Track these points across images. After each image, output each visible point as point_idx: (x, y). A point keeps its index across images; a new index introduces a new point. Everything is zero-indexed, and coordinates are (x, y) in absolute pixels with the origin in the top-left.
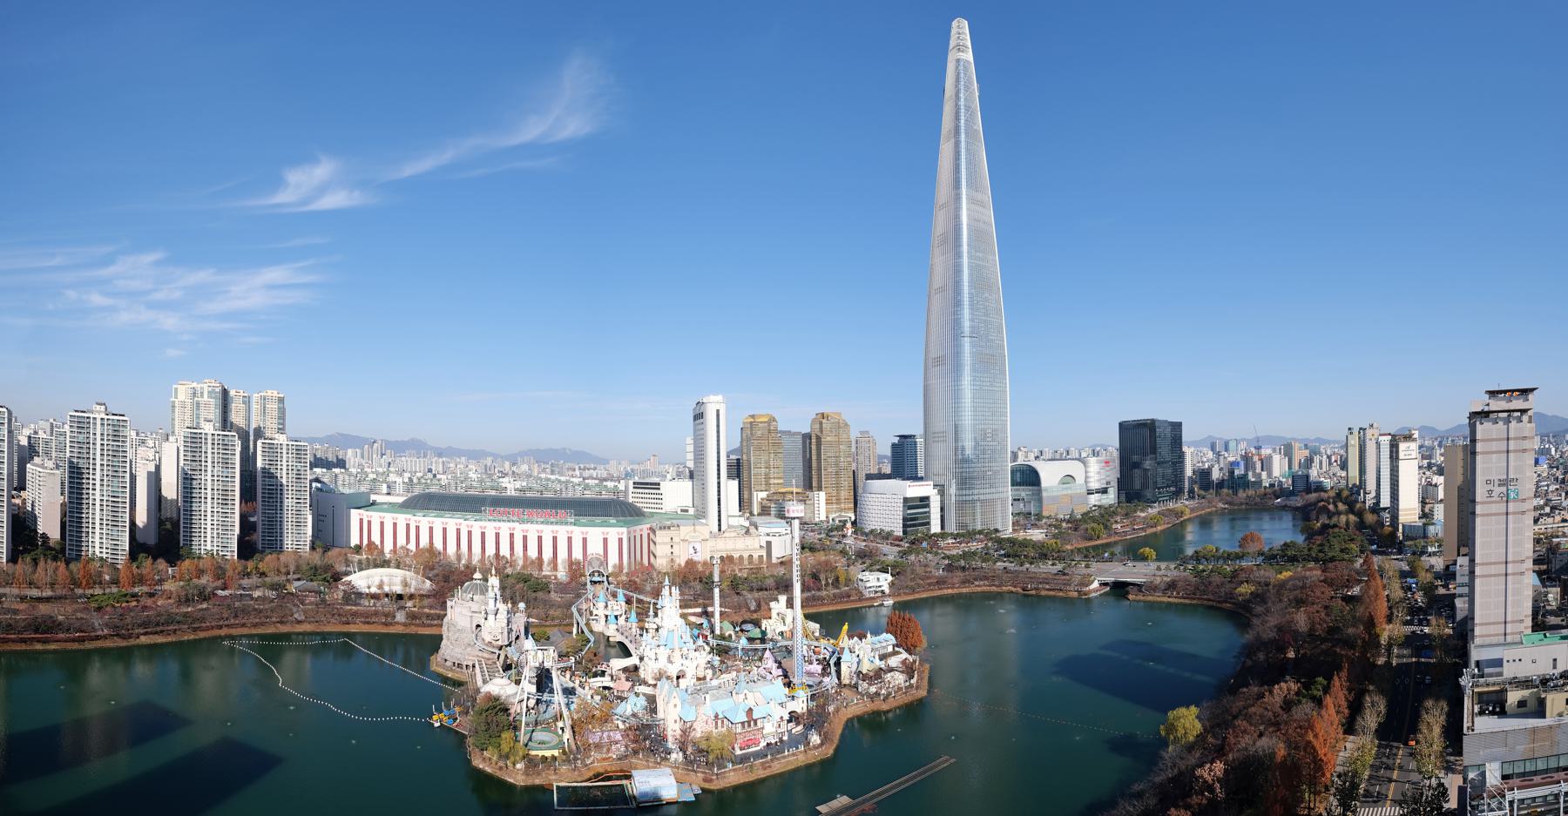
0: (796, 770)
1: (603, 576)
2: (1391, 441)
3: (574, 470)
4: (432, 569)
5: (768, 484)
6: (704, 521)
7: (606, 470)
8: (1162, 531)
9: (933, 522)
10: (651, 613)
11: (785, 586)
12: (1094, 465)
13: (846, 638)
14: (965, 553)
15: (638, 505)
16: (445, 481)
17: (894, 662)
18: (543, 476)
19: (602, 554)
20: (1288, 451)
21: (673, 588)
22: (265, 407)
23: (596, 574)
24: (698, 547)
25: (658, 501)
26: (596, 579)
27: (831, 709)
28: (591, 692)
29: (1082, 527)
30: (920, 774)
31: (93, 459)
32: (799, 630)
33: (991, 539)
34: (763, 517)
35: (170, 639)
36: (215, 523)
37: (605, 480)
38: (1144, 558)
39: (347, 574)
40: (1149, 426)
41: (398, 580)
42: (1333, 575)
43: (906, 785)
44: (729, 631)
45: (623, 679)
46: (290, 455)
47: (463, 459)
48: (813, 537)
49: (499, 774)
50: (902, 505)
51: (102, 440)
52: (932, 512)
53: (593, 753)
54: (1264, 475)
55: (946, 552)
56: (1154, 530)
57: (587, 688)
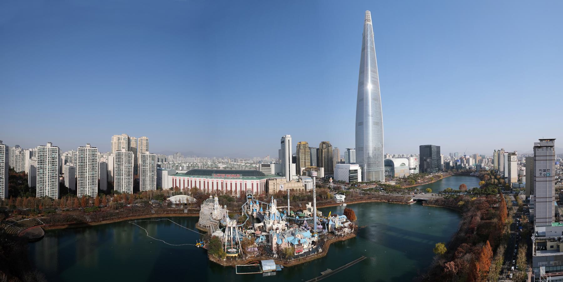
0: (314, 260)
1: (252, 196)
2: (508, 155)
3: (242, 161)
5: (305, 165)
6: (284, 177)
8: (434, 182)
9: (358, 178)
10: (267, 208)
12: (412, 160)
13: (330, 216)
14: (369, 189)
15: (263, 172)
18: (232, 163)
19: (251, 188)
20: (475, 157)
21: (275, 200)
22: (142, 143)
23: (250, 195)
24: (283, 186)
25: (270, 171)
26: (250, 197)
27: (325, 240)
28: (248, 235)
29: (408, 181)
33: (378, 184)
34: (304, 176)
35: (111, 222)
36: (126, 182)
37: (253, 164)
38: (428, 192)
39: (169, 197)
40: (430, 147)
41: (185, 199)
44: (293, 214)
45: (258, 230)
46: (150, 159)
48: (320, 183)
49: (218, 262)
51: (89, 156)
52: (358, 175)
54: (467, 165)
56: (431, 182)
57: (247, 233)
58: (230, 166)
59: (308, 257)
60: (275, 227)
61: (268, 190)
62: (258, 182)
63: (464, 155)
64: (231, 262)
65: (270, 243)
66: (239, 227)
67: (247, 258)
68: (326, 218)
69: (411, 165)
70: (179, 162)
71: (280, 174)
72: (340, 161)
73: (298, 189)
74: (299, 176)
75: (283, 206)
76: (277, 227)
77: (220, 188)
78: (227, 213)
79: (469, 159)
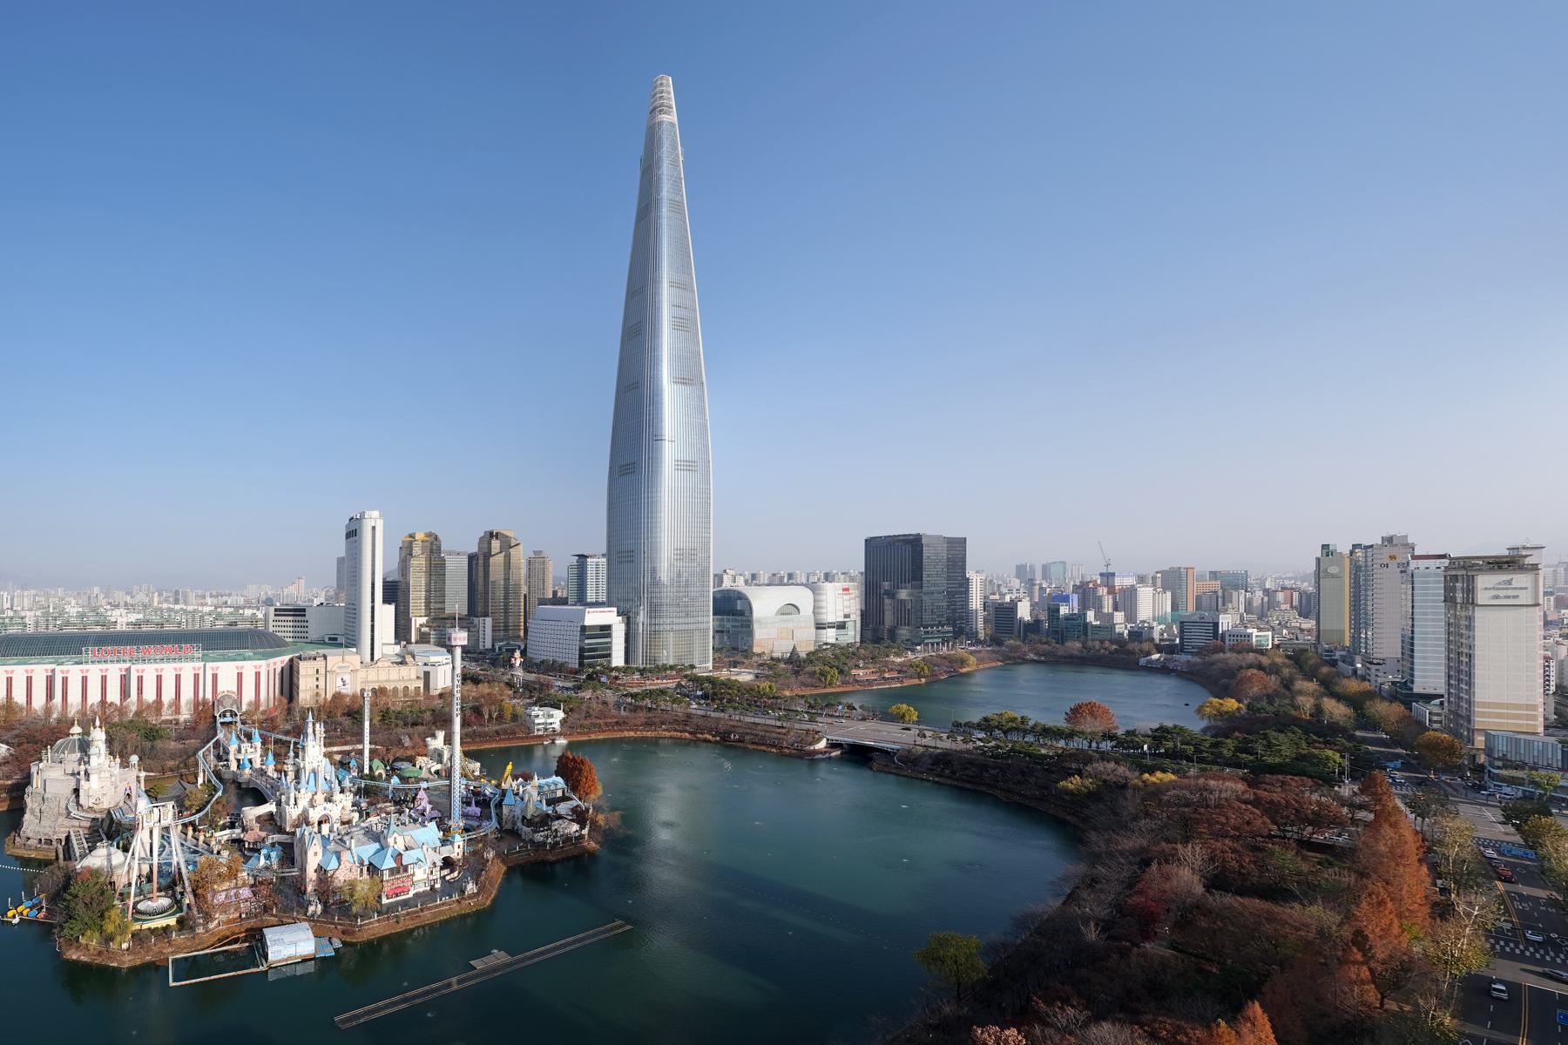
1: (236, 715)
3: (204, 597)
6: (354, 650)
7: (242, 596)
9: (614, 655)
10: (292, 754)
11: (443, 721)
13: (510, 779)
15: (280, 634)
17: (563, 808)
18: (165, 606)
19: (235, 690)
21: (318, 725)
23: (228, 714)
24: (347, 678)
26: (228, 719)
32: (457, 768)
33: (686, 676)
37: (243, 608)
40: (914, 544)
42: (1276, 797)
44: (380, 770)
49: (98, 960)
50: (579, 633)
53: (217, 915)
54: (1119, 617)
58: (155, 618)
59: (429, 909)
60: (315, 815)
61: (295, 694)
62: (260, 667)
63: (1101, 575)
64: (149, 950)
65: (296, 869)
66: (185, 826)
67: (212, 926)
68: (493, 782)
69: (824, 611)
72: (551, 596)
74: (405, 647)
75: (346, 744)
76: (325, 815)
77: (114, 696)
78: (139, 782)
79: (1130, 593)
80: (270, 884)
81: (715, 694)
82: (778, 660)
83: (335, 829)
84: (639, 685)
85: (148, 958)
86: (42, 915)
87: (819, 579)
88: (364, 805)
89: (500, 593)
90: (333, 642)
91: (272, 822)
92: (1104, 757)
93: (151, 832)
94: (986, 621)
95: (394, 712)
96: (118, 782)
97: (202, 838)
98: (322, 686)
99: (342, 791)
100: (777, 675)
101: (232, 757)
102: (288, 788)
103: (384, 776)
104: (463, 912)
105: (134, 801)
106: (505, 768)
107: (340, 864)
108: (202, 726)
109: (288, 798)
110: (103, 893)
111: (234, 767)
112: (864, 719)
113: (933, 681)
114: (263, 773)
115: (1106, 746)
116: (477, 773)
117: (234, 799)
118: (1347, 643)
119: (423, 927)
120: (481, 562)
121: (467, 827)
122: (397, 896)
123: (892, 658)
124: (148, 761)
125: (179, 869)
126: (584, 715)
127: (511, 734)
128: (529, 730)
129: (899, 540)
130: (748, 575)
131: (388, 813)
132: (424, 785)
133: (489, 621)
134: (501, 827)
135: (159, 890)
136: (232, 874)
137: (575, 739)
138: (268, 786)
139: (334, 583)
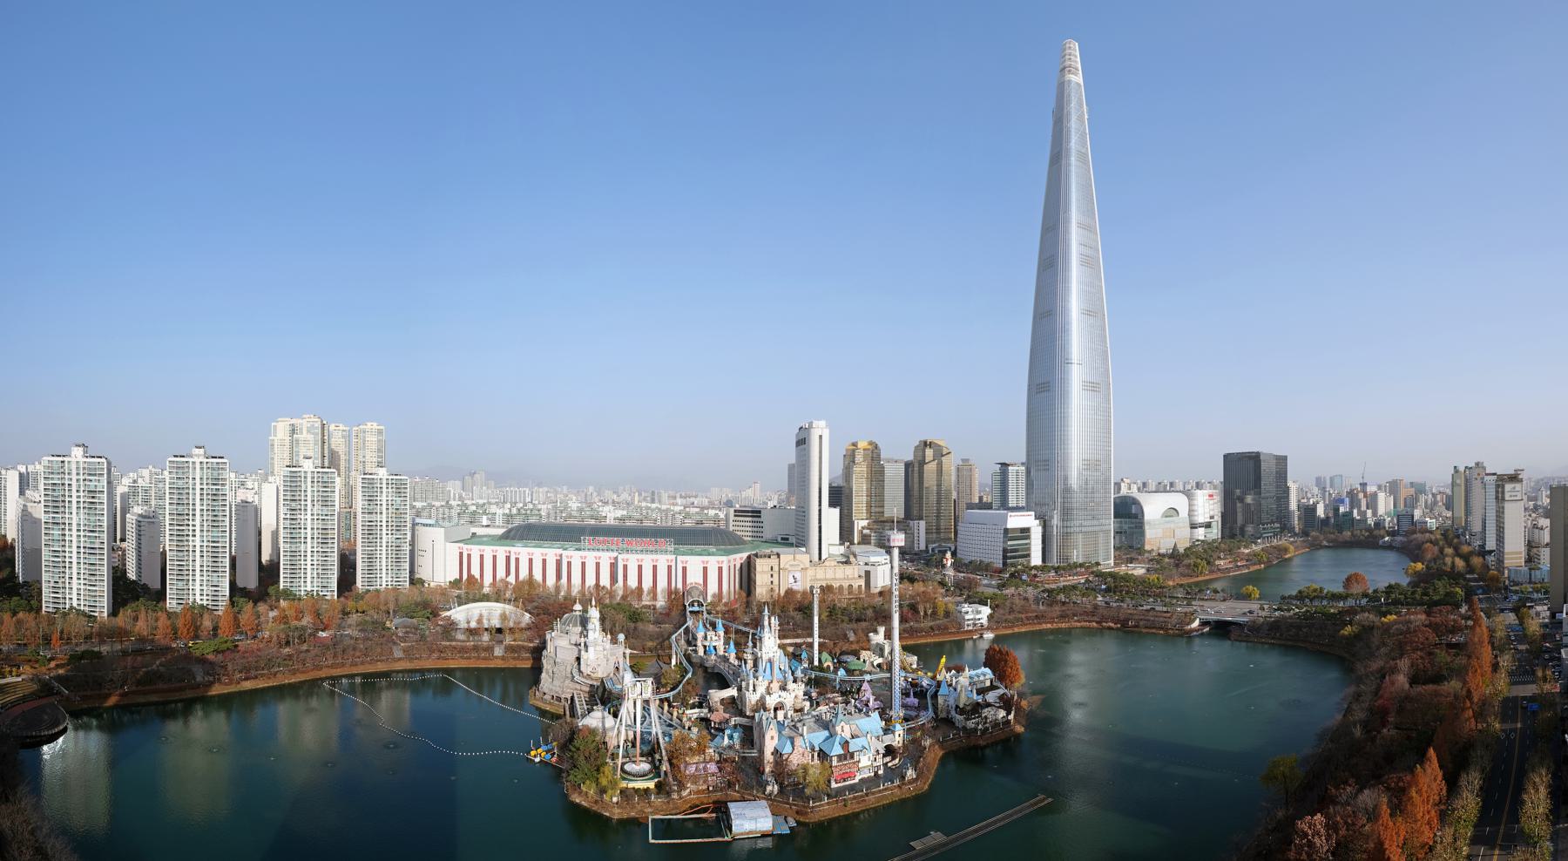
1: (702, 605)
3: (675, 498)
4: (531, 601)
6: (804, 549)
7: (706, 497)
9: (1033, 555)
10: (750, 644)
11: (883, 617)
12: (1201, 497)
13: (944, 670)
15: (739, 533)
16: (545, 512)
17: (991, 697)
18: (644, 504)
19: (702, 582)
21: (773, 618)
23: (696, 604)
24: (798, 575)
26: (696, 608)
30: (1016, 813)
31: (193, 489)
33: (1092, 573)
34: (863, 546)
37: (708, 509)
42: (1438, 620)
43: (1002, 823)
44: (828, 663)
47: (565, 488)
53: (689, 785)
54: (1369, 513)
55: (1046, 586)
58: (636, 515)
59: (873, 793)
60: (771, 702)
62: (722, 562)
63: (1361, 484)
64: (633, 807)
65: (755, 751)
66: (662, 701)
67: (685, 793)
69: (1196, 513)
70: (481, 502)
71: (790, 541)
72: (977, 501)
73: (846, 585)
74: (848, 547)
75: (797, 637)
77: (605, 581)
78: (625, 657)
80: (733, 761)
81: (1116, 587)
82: (1163, 556)
83: (789, 716)
84: (1055, 582)
85: (633, 814)
86: (554, 759)
87: (1192, 487)
88: (814, 695)
89: (933, 498)
90: (785, 541)
91: (734, 705)
92: (1363, 609)
93: (635, 703)
94: (1299, 519)
95: (840, 608)
96: (609, 656)
97: (675, 714)
98: (776, 582)
99: (795, 681)
100: (1163, 568)
101: (699, 643)
102: (748, 675)
103: (832, 668)
104: (904, 796)
105: (621, 674)
106: (939, 662)
107: (794, 749)
108: (675, 613)
109: (748, 684)
110: (598, 751)
111: (701, 652)
112: (1224, 600)
113: (1269, 566)
114: (725, 659)
115: (1364, 601)
116: (915, 666)
117: (701, 681)
118: (1463, 525)
119: (868, 810)
120: (916, 469)
121: (907, 717)
122: (845, 781)
123: (1243, 550)
124: (633, 641)
125: (658, 739)
126: (1007, 611)
127: (944, 629)
128: (960, 625)
129: (1246, 457)
130: (1140, 483)
131: (836, 703)
132: (868, 677)
133: (923, 523)
134: (937, 717)
135: (642, 755)
136: (701, 750)
137: (1001, 633)
138: (731, 672)
139: (785, 487)
